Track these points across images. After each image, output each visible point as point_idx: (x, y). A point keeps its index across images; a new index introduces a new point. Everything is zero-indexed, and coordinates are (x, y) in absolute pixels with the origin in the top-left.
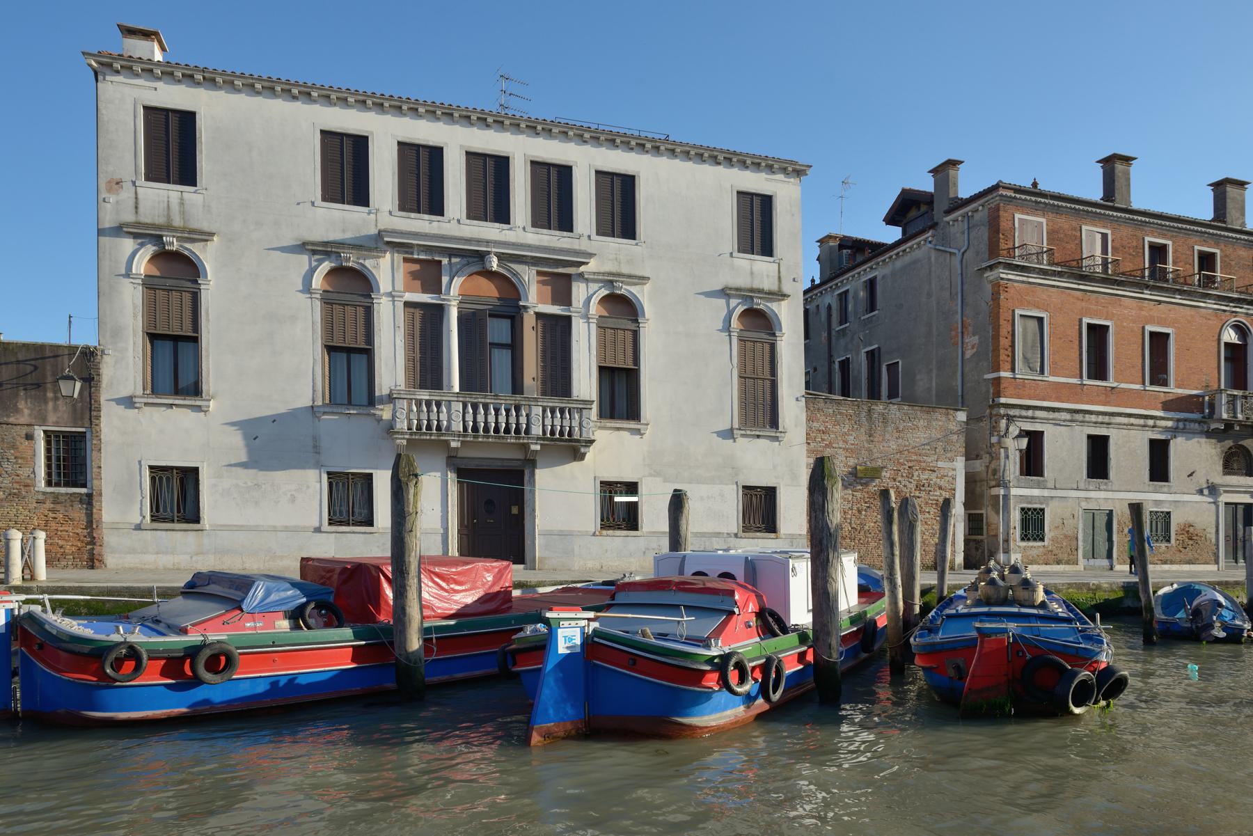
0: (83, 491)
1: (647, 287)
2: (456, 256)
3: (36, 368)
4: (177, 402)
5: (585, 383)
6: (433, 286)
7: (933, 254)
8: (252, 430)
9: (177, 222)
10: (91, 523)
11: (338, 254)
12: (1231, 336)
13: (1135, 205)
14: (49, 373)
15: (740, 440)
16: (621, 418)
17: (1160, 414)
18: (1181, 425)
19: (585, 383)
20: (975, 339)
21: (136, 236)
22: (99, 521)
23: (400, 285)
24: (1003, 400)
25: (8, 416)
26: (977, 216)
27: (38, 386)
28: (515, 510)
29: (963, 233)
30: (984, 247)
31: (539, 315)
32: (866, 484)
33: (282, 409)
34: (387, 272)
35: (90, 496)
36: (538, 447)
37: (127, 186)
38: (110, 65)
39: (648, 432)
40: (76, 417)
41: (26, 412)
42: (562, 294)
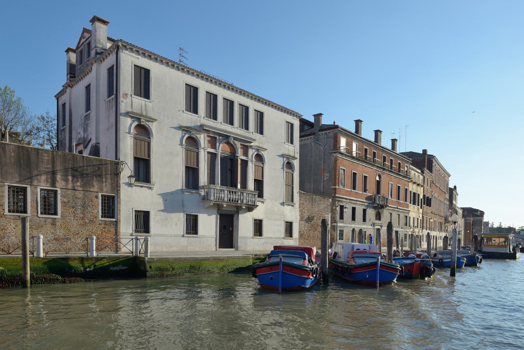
0: (114, 220)
1: (155, 123)
2: (221, 136)
3: (99, 168)
4: (144, 185)
5: (251, 185)
6: (214, 146)
7: (313, 144)
8: (165, 196)
9: (144, 114)
10: (117, 233)
11: (190, 132)
12: (378, 179)
13: (382, 145)
14: (104, 171)
15: (285, 206)
16: (141, 181)
17: (365, 201)
19: (251, 185)
20: (328, 175)
21: (132, 117)
22: (120, 232)
23: (206, 146)
24: (337, 195)
25: (90, 188)
26: (330, 135)
27: (100, 176)
28: (231, 229)
29: (325, 139)
30: (332, 145)
31: (242, 160)
32: (311, 222)
33: (174, 190)
34: (203, 139)
35: (116, 222)
36: (244, 207)
37: (129, 96)
38: (125, 47)
39: (266, 202)
40: (113, 190)
41: (96, 186)
42: (246, 154)
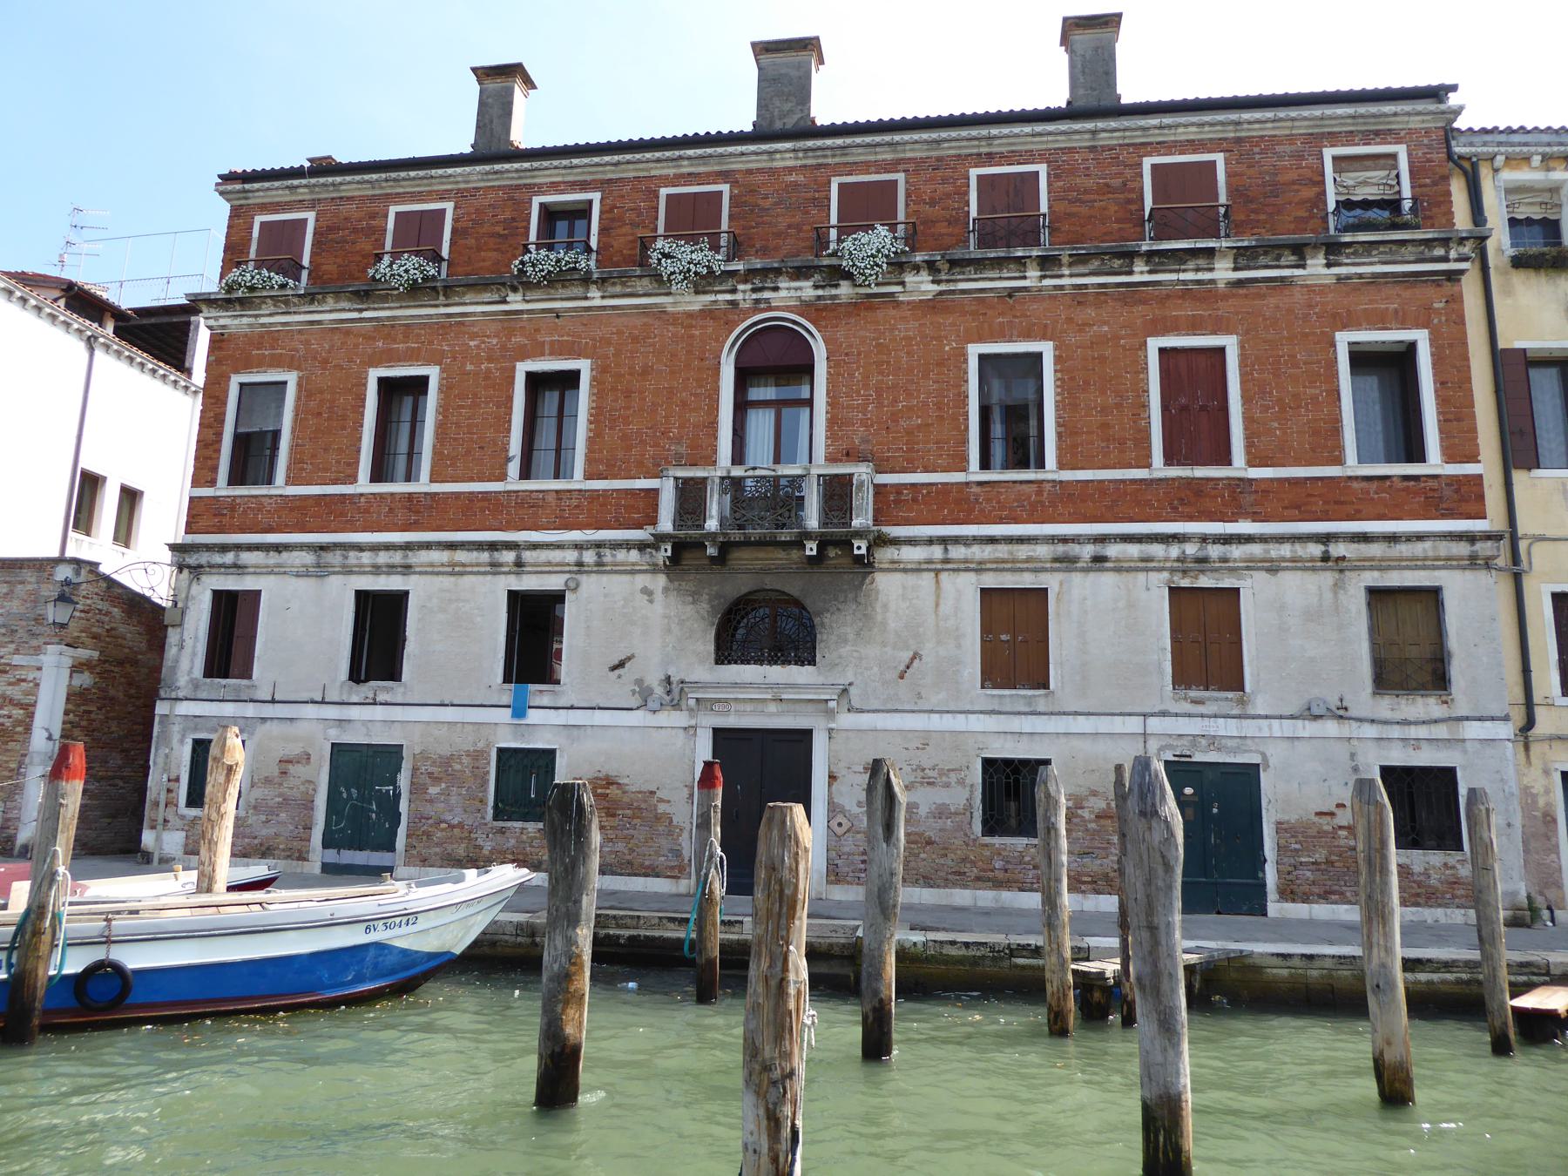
13: (1126, 99)
18: (589, 557)
